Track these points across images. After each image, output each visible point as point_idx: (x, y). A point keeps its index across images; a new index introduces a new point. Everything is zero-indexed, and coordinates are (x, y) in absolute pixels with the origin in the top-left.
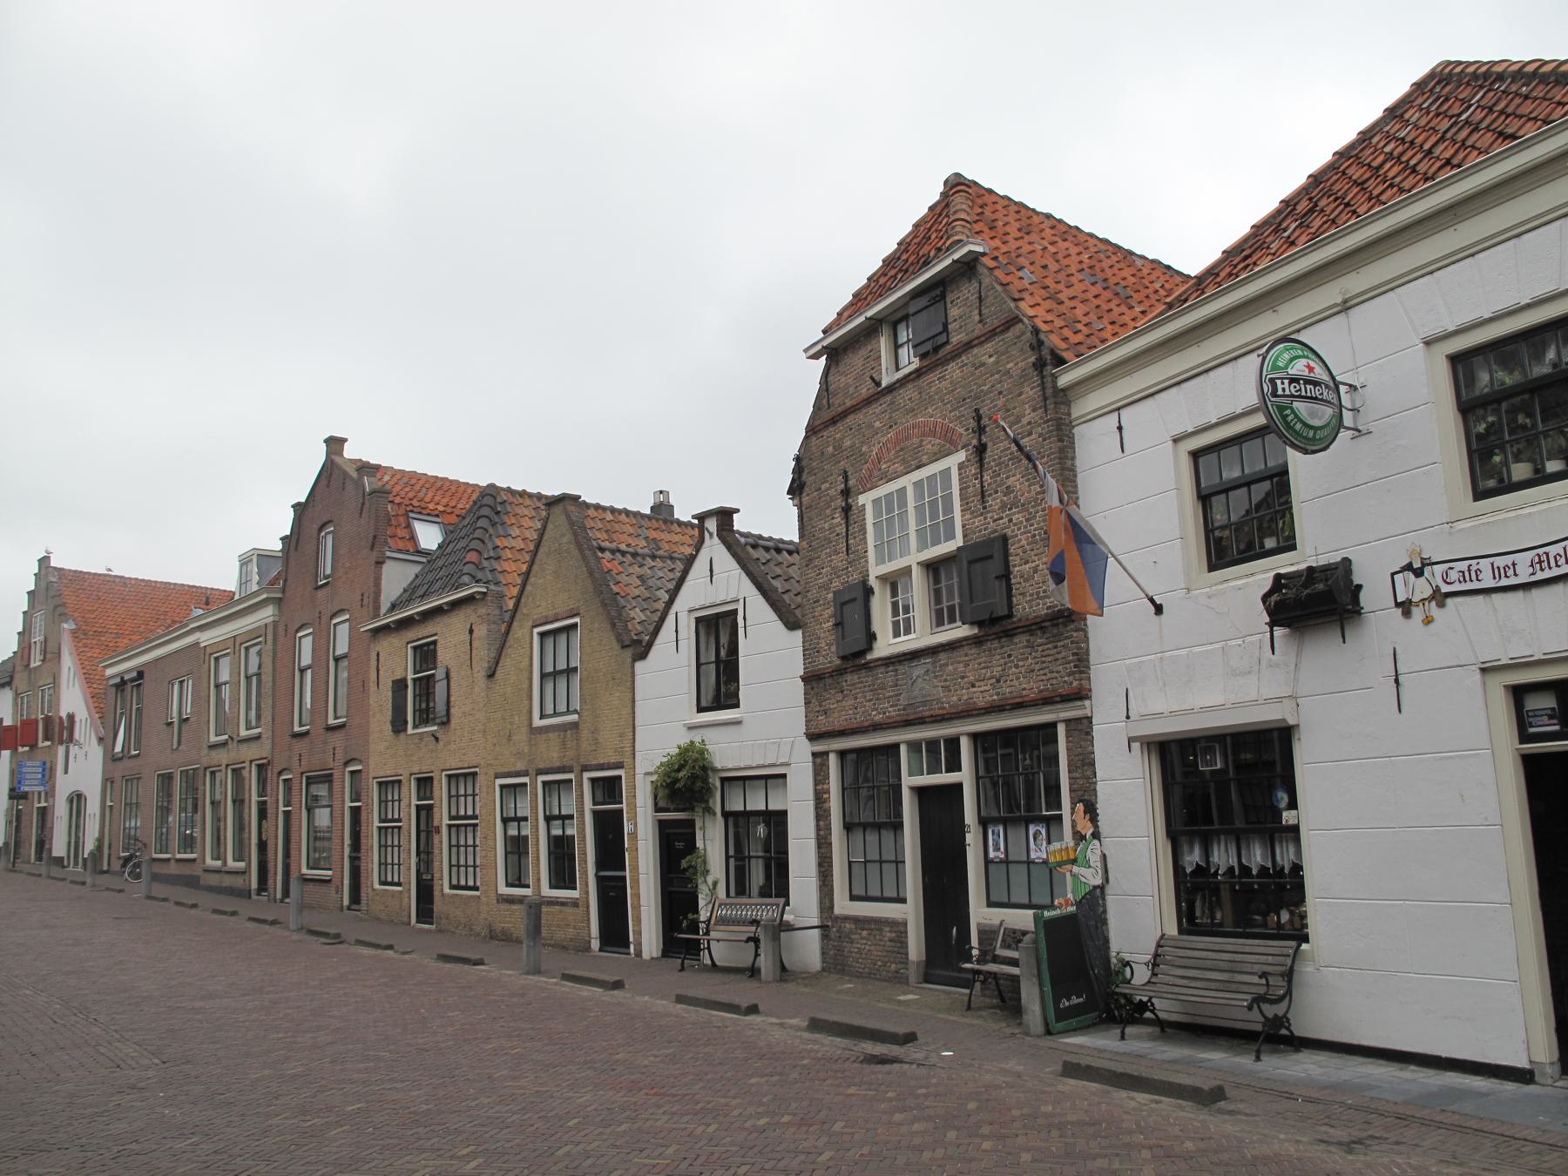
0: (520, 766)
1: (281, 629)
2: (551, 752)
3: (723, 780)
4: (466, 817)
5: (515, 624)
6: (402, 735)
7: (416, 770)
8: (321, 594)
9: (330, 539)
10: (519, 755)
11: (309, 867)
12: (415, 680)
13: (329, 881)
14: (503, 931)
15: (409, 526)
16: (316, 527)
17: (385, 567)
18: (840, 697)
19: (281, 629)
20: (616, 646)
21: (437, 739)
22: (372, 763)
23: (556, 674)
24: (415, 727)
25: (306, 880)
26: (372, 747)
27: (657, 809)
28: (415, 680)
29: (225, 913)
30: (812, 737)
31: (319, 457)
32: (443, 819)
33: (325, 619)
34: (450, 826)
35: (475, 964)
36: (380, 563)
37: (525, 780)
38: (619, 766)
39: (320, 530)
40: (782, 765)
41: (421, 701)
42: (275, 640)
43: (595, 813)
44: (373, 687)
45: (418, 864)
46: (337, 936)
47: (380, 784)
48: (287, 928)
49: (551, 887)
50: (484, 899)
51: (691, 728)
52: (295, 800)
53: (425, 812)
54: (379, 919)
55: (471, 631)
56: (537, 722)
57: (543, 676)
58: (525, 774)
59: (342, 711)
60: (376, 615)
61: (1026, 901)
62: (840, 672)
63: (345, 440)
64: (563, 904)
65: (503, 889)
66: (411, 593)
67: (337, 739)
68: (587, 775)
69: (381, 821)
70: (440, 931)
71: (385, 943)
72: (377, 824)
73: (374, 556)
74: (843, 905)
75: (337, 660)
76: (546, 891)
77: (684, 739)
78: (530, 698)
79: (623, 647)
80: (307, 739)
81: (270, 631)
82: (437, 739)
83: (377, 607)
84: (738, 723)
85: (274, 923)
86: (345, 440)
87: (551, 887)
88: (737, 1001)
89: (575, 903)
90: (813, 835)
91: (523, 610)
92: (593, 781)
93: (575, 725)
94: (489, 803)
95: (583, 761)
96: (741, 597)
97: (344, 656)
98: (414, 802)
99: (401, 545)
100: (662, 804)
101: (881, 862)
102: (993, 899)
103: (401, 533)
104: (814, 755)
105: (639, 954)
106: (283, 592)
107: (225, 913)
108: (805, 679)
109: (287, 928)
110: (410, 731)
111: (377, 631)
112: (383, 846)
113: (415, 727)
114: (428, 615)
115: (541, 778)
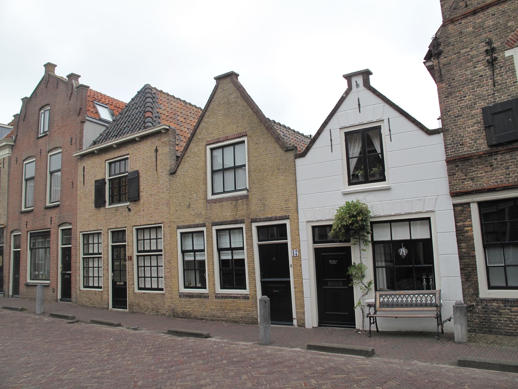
0: (198, 221)
1: (13, 160)
2: (226, 213)
3: (372, 223)
4: (150, 251)
5: (191, 145)
6: (102, 209)
7: (112, 227)
8: (40, 141)
9: (47, 114)
10: (198, 215)
11: (31, 279)
12: (110, 180)
13: (48, 286)
14: (183, 313)
15: (94, 107)
16: (37, 108)
17: (85, 124)
18: (490, 169)
19: (13, 160)
20: (280, 151)
21: (130, 210)
22: (79, 224)
23: (224, 170)
24: (110, 204)
25: (28, 285)
26: (78, 216)
27: (315, 242)
28: (110, 180)
29: (17, 309)
30: (454, 195)
31: (41, 73)
32: (132, 251)
33: (43, 153)
34: (138, 256)
35: (206, 337)
36: (83, 122)
37: (204, 229)
38: (287, 218)
39: (41, 109)
40: (427, 212)
41: (123, 189)
42: (9, 166)
43: (260, 246)
44: (80, 184)
45: (113, 277)
46: (73, 318)
47: (84, 235)
48: (35, 313)
49: (222, 288)
50: (167, 295)
51: (345, 194)
52: (23, 245)
53: (67, 253)
54: (83, 306)
55: (156, 150)
56: (210, 197)
57: (213, 172)
58: (204, 225)
59: (29, 204)
60: (81, 149)
61: (504, 285)
62: (490, 154)
63: (56, 66)
64: (231, 297)
65: (183, 290)
66: (105, 137)
67: (53, 213)
68: (254, 225)
69: (84, 254)
70: (133, 313)
71: (116, 323)
72: (82, 256)
73: (80, 118)
74: (484, 293)
75: (26, 180)
76: (219, 291)
77: (342, 202)
78: (206, 184)
79: (287, 151)
80: (32, 214)
81: (6, 162)
82: (130, 210)
83: (81, 145)
84: (388, 189)
85: (22, 310)
86: (56, 66)
87: (222, 288)
88: (17, 307)
89: (246, 297)
90: (456, 251)
91: (198, 136)
92: (258, 228)
93: (246, 197)
94: (170, 243)
95: (252, 216)
96: (385, 118)
97: (32, 178)
98: (13, 250)
99: (92, 115)
100: (316, 240)
101: (151, 267)
102: (492, 285)
103: (92, 110)
104: (455, 205)
105: (302, 325)
106: (15, 142)
107: (17, 309)
108: (449, 162)
109: (35, 313)
110: (107, 206)
111: (83, 156)
112: (86, 269)
113: (110, 204)
114: (120, 145)
115: (215, 228)
